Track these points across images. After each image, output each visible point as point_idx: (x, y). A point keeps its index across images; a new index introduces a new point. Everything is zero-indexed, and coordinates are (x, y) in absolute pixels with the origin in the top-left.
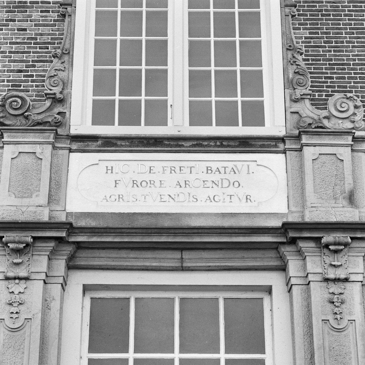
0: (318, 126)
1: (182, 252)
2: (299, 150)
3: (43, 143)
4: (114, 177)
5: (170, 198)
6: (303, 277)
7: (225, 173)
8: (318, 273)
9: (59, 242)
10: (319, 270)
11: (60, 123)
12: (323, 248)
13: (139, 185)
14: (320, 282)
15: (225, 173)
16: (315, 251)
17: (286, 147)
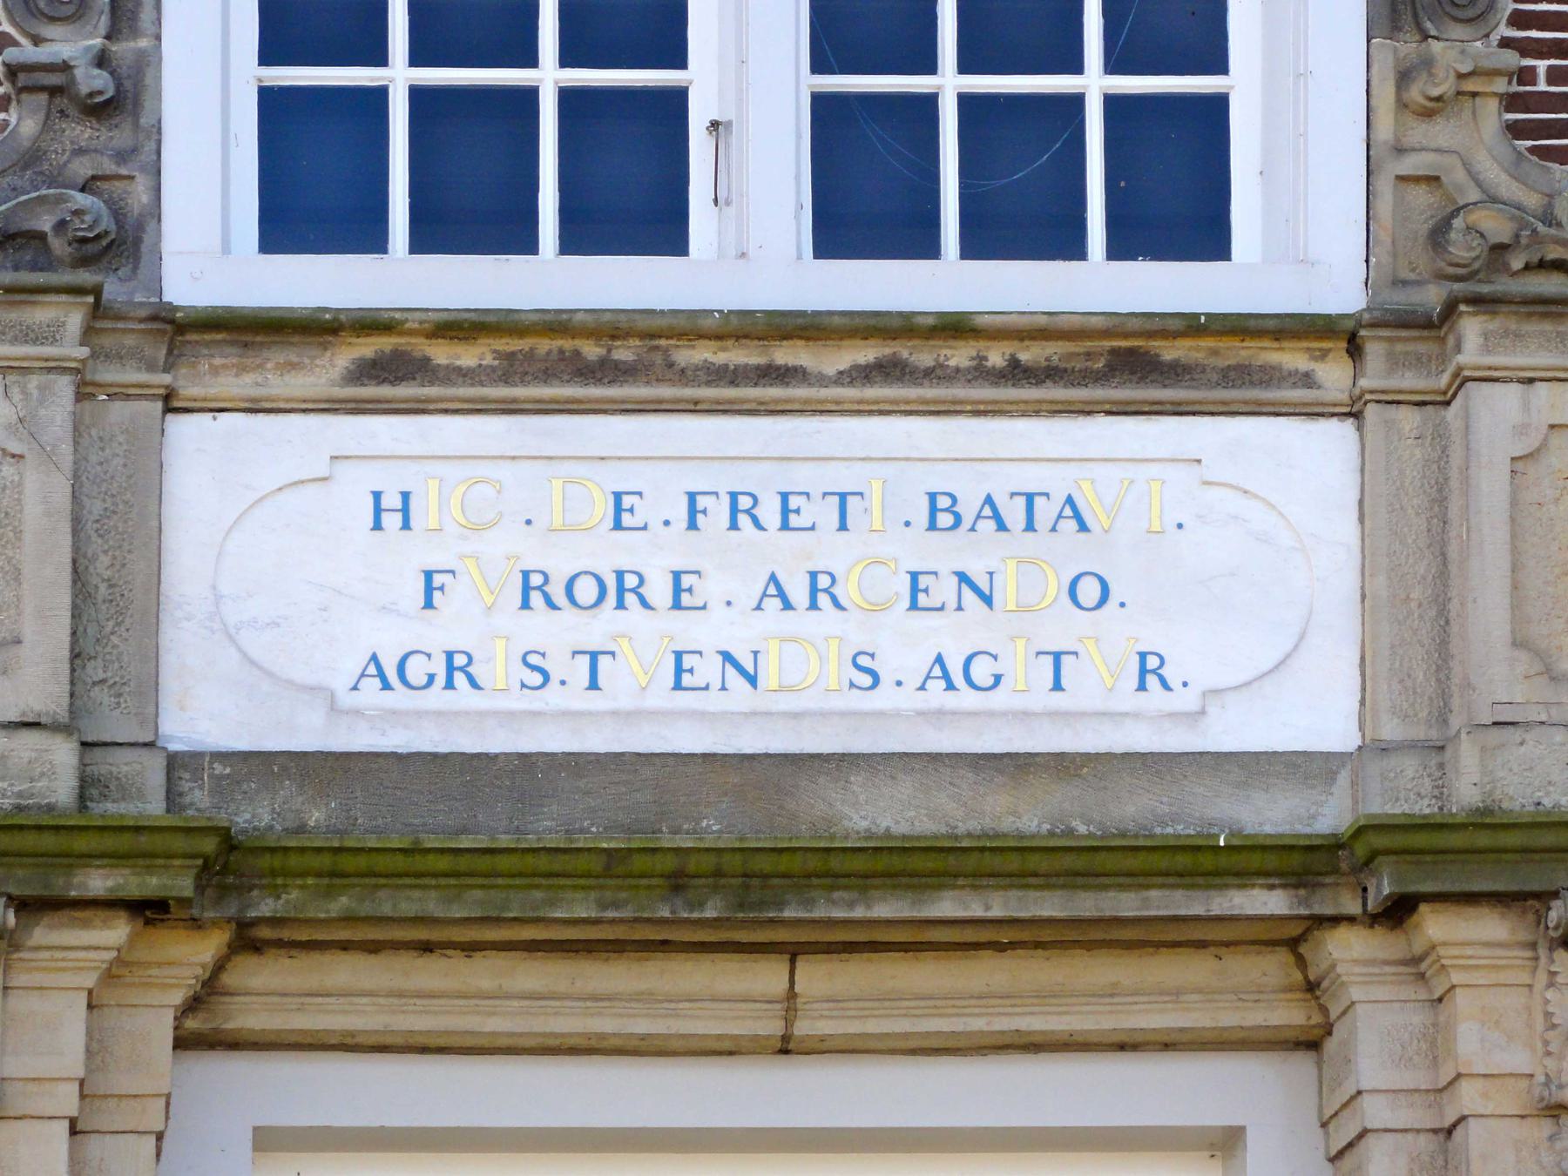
0: (1541, 260)
1: (793, 962)
2: (1439, 398)
3: (25, 364)
4: (419, 552)
5: (731, 672)
6: (1428, 1091)
7: (1030, 527)
8: (1511, 1075)
9: (148, 922)
10: (1518, 1059)
11: (104, 243)
12: (1551, 949)
13: (560, 598)
14: (1518, 1120)
15: (1030, 527)
16: (1503, 962)
17: (1363, 383)
